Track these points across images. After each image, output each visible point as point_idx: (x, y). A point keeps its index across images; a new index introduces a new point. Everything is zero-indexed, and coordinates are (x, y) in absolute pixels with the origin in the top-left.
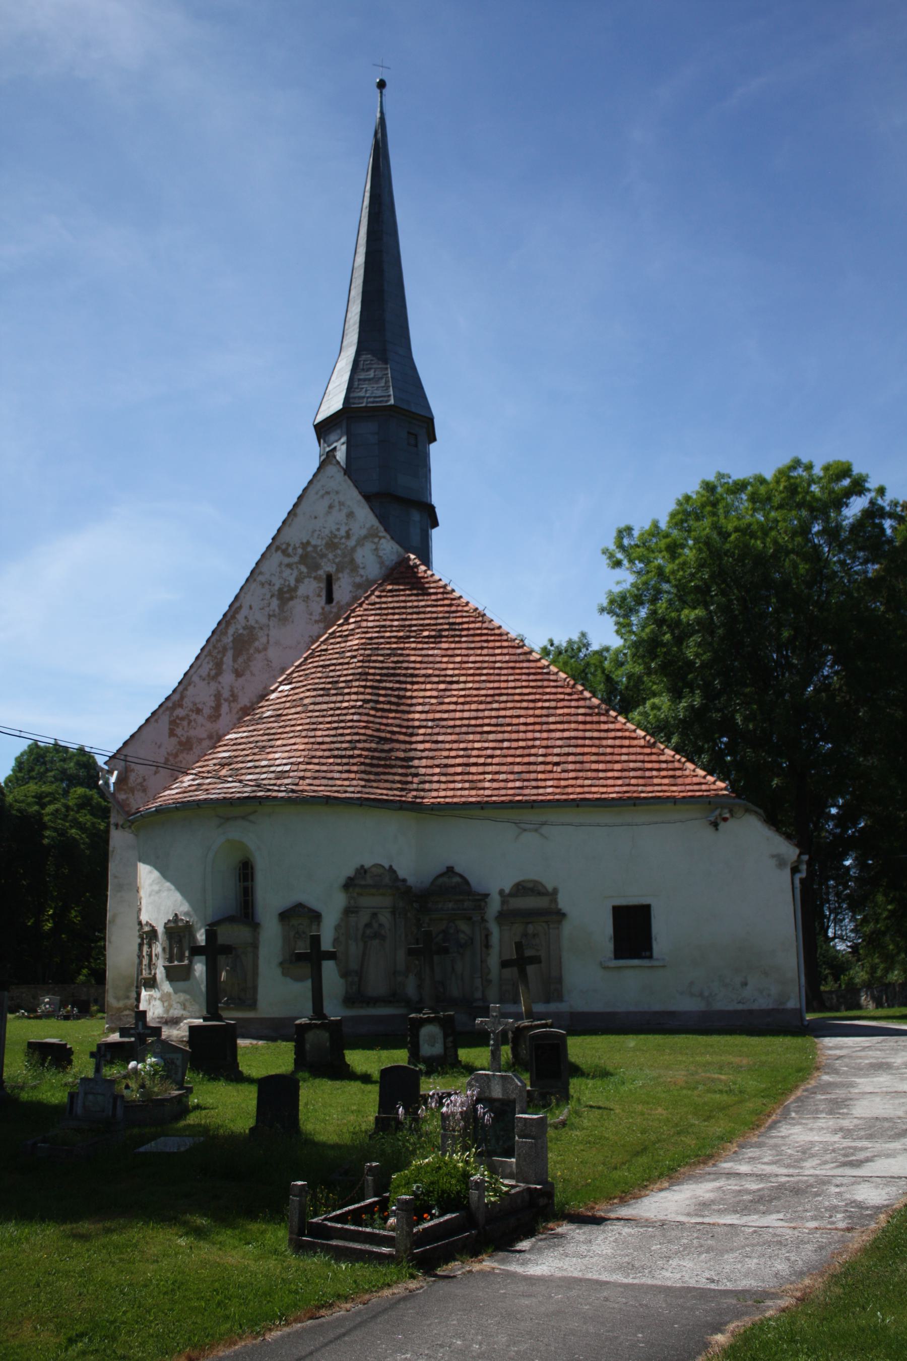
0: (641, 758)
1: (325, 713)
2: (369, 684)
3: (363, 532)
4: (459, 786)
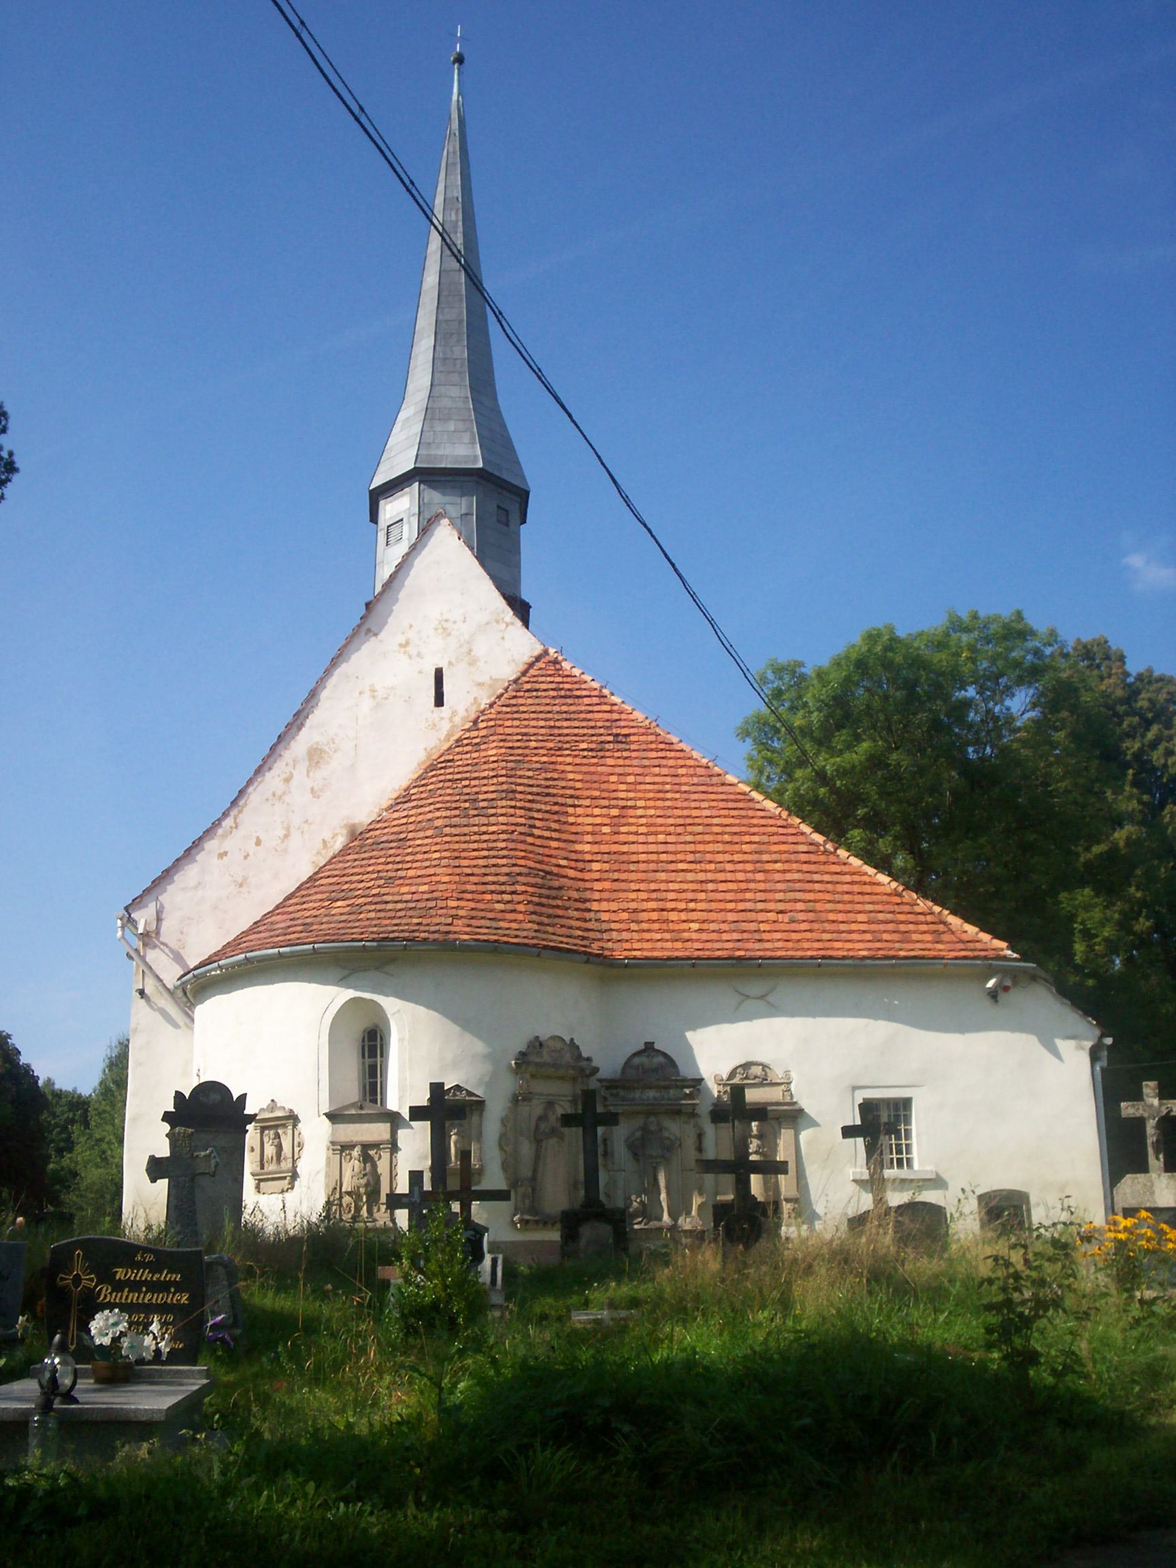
1: (467, 838)
2: (518, 804)
4: (658, 936)
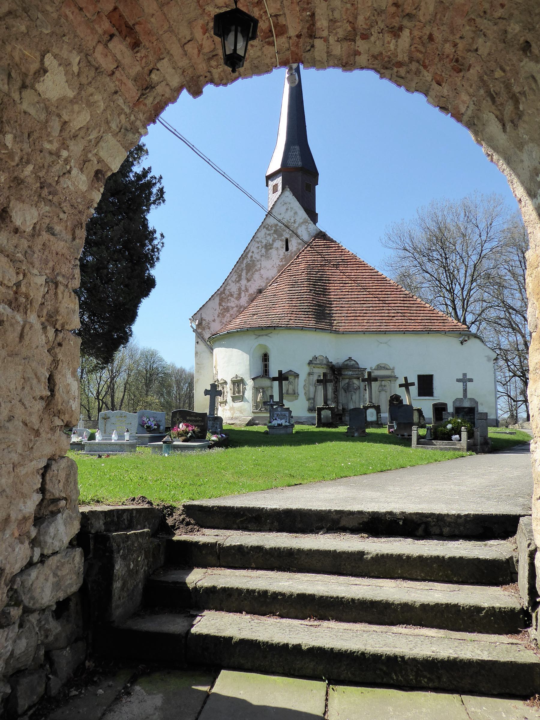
0: (429, 315)
3: (301, 221)
